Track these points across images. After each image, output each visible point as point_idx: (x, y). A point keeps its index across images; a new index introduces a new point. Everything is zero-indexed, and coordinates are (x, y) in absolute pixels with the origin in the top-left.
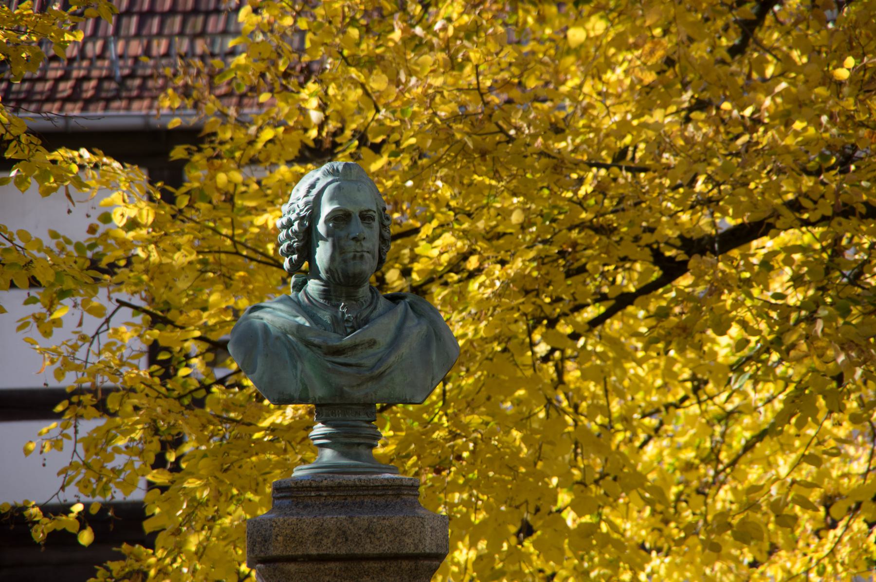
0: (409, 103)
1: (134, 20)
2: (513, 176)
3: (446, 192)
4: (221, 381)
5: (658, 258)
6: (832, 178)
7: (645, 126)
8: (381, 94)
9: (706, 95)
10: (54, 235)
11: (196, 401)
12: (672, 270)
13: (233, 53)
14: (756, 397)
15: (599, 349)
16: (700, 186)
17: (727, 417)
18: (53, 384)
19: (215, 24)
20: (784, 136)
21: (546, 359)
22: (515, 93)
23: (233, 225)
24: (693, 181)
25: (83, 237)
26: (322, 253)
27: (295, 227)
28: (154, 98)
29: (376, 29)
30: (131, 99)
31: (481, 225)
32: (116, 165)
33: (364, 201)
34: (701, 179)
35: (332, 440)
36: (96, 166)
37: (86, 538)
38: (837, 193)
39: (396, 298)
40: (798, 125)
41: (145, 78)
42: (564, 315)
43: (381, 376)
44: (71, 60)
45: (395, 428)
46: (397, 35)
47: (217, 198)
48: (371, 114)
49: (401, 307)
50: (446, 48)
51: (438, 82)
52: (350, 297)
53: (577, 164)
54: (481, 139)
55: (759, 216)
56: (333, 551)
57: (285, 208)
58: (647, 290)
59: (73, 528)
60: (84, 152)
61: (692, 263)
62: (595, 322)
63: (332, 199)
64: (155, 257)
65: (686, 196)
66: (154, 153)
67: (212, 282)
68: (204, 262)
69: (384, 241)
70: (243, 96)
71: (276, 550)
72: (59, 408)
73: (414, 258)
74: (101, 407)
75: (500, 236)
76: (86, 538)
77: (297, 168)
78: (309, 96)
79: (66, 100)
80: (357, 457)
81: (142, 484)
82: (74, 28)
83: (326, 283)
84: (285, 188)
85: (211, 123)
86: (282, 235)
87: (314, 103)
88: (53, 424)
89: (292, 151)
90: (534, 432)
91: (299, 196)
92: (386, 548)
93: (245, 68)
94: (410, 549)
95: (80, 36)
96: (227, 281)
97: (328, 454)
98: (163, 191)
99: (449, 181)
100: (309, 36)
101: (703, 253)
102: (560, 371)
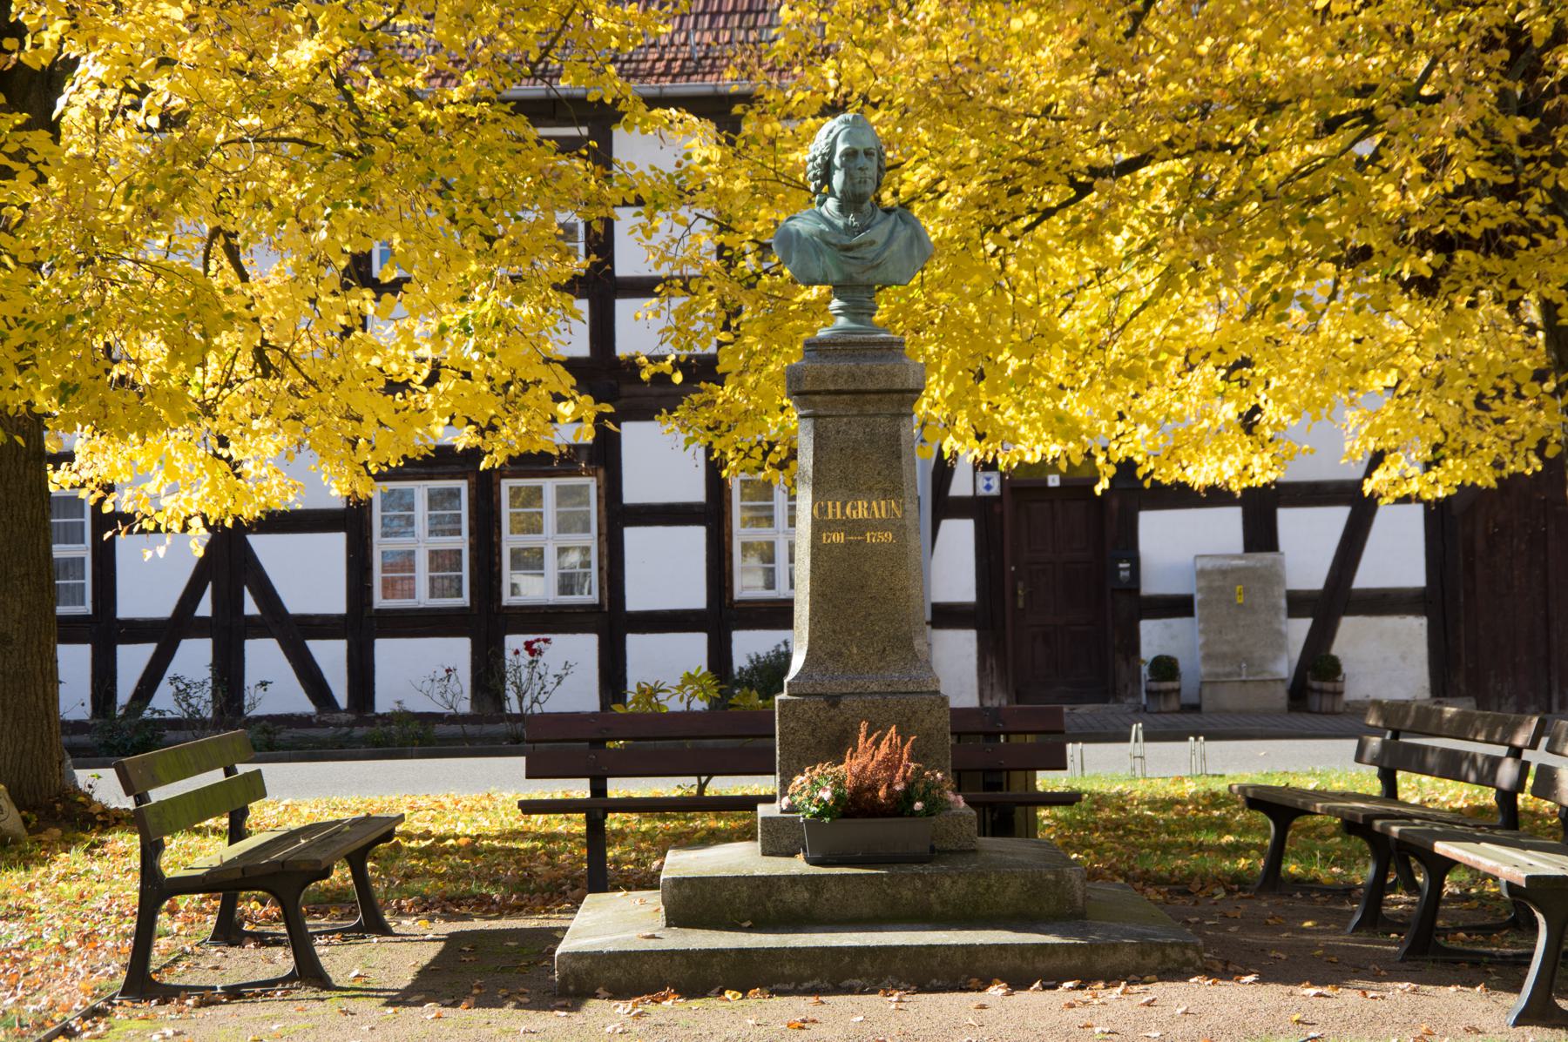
0: (899, 72)
1: (707, 18)
2: (972, 125)
3: (924, 136)
4: (766, 271)
5: (1072, 182)
6: (1195, 124)
7: (1065, 87)
8: (880, 67)
9: (1107, 66)
10: (653, 168)
11: (750, 283)
12: (1083, 190)
13: (775, 39)
14: (1140, 279)
15: (1031, 247)
16: (1103, 131)
17: (1120, 295)
18: (655, 273)
19: (763, 20)
20: (1162, 94)
21: (993, 254)
22: (973, 66)
23: (775, 161)
24: (1097, 128)
25: (672, 170)
26: (838, 179)
27: (819, 160)
28: (720, 73)
29: (876, 20)
30: (704, 74)
31: (949, 159)
32: (695, 119)
33: (867, 142)
34: (1104, 125)
35: (845, 311)
36: (681, 121)
37: (678, 378)
38: (1198, 134)
39: (889, 211)
40: (1171, 86)
41: (714, 59)
42: (1006, 223)
43: (878, 266)
44: (664, 47)
45: (888, 302)
46: (890, 25)
47: (763, 142)
48: (871, 81)
49: (893, 217)
50: (925, 33)
51: (919, 57)
52: (857, 210)
53: (1016, 116)
54: (950, 98)
55: (1145, 150)
56: (845, 387)
57: (812, 147)
58: (1064, 205)
59: (668, 371)
60: (672, 110)
61: (1096, 184)
62: (1031, 227)
63: (844, 141)
64: (721, 184)
65: (1093, 138)
66: (720, 111)
67: (760, 200)
68: (755, 187)
69: (882, 170)
70: (781, 71)
71: (806, 387)
72: (658, 289)
73: (902, 182)
74: (686, 288)
75: (961, 167)
76: (678, 378)
77: (819, 120)
78: (828, 68)
79: (660, 75)
80: (862, 322)
81: (714, 341)
82: (666, 22)
83: (840, 200)
84: (812, 132)
85: (761, 88)
86: (810, 166)
87: (831, 74)
88: (655, 300)
89: (816, 109)
90: (985, 304)
91: (819, 144)
92: (882, 385)
93: (784, 49)
94: (898, 386)
95: (669, 28)
96: (771, 200)
97: (842, 321)
98: (727, 137)
99: (927, 128)
100: (828, 27)
101: (1104, 177)
102: (1003, 265)
